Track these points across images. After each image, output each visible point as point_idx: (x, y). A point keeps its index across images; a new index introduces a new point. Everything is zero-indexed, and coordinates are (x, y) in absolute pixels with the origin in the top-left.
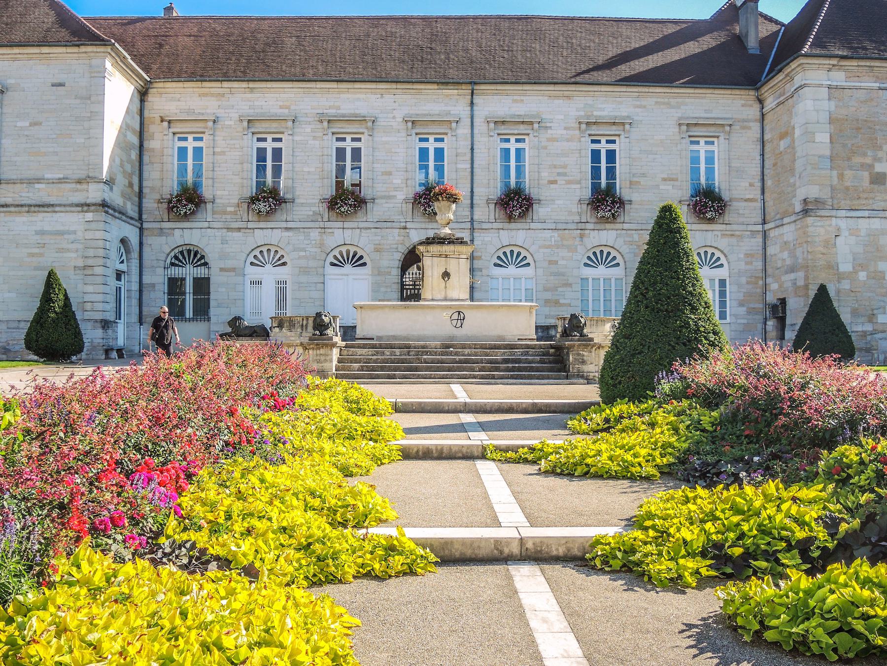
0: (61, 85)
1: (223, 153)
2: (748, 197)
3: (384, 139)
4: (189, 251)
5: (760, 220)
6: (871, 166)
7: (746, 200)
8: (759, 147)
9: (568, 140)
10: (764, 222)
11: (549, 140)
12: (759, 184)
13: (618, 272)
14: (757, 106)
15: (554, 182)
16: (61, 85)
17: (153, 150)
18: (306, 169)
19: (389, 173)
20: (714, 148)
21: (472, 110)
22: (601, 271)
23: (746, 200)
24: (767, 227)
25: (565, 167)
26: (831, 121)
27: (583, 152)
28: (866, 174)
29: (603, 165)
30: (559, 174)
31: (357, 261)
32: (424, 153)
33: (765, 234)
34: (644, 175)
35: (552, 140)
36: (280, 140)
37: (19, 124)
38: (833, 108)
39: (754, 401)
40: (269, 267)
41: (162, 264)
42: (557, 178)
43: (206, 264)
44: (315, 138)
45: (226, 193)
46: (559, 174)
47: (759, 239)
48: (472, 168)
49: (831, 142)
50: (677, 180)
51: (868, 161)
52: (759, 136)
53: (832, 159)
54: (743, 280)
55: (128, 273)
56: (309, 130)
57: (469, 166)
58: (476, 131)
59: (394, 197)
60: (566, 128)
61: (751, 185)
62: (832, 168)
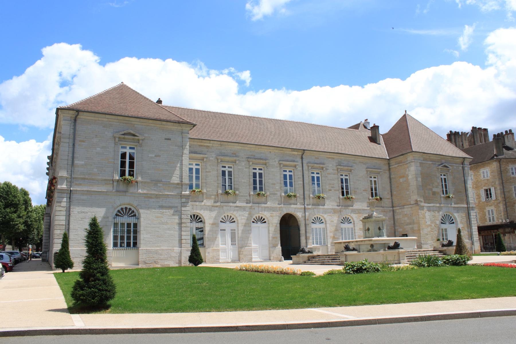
5: (391, 206)
6: (431, 189)
15: (330, 190)
18: (243, 181)
19: (274, 184)
21: (302, 160)
25: (333, 184)
28: (431, 192)
29: (258, 179)
30: (332, 187)
31: (262, 220)
32: (224, 173)
33: (393, 211)
37: (150, 155)
39: (112, 283)
42: (332, 189)
44: (246, 168)
45: (211, 189)
46: (332, 187)
47: (392, 213)
51: (431, 187)
56: (243, 164)
57: (302, 183)
59: (276, 194)
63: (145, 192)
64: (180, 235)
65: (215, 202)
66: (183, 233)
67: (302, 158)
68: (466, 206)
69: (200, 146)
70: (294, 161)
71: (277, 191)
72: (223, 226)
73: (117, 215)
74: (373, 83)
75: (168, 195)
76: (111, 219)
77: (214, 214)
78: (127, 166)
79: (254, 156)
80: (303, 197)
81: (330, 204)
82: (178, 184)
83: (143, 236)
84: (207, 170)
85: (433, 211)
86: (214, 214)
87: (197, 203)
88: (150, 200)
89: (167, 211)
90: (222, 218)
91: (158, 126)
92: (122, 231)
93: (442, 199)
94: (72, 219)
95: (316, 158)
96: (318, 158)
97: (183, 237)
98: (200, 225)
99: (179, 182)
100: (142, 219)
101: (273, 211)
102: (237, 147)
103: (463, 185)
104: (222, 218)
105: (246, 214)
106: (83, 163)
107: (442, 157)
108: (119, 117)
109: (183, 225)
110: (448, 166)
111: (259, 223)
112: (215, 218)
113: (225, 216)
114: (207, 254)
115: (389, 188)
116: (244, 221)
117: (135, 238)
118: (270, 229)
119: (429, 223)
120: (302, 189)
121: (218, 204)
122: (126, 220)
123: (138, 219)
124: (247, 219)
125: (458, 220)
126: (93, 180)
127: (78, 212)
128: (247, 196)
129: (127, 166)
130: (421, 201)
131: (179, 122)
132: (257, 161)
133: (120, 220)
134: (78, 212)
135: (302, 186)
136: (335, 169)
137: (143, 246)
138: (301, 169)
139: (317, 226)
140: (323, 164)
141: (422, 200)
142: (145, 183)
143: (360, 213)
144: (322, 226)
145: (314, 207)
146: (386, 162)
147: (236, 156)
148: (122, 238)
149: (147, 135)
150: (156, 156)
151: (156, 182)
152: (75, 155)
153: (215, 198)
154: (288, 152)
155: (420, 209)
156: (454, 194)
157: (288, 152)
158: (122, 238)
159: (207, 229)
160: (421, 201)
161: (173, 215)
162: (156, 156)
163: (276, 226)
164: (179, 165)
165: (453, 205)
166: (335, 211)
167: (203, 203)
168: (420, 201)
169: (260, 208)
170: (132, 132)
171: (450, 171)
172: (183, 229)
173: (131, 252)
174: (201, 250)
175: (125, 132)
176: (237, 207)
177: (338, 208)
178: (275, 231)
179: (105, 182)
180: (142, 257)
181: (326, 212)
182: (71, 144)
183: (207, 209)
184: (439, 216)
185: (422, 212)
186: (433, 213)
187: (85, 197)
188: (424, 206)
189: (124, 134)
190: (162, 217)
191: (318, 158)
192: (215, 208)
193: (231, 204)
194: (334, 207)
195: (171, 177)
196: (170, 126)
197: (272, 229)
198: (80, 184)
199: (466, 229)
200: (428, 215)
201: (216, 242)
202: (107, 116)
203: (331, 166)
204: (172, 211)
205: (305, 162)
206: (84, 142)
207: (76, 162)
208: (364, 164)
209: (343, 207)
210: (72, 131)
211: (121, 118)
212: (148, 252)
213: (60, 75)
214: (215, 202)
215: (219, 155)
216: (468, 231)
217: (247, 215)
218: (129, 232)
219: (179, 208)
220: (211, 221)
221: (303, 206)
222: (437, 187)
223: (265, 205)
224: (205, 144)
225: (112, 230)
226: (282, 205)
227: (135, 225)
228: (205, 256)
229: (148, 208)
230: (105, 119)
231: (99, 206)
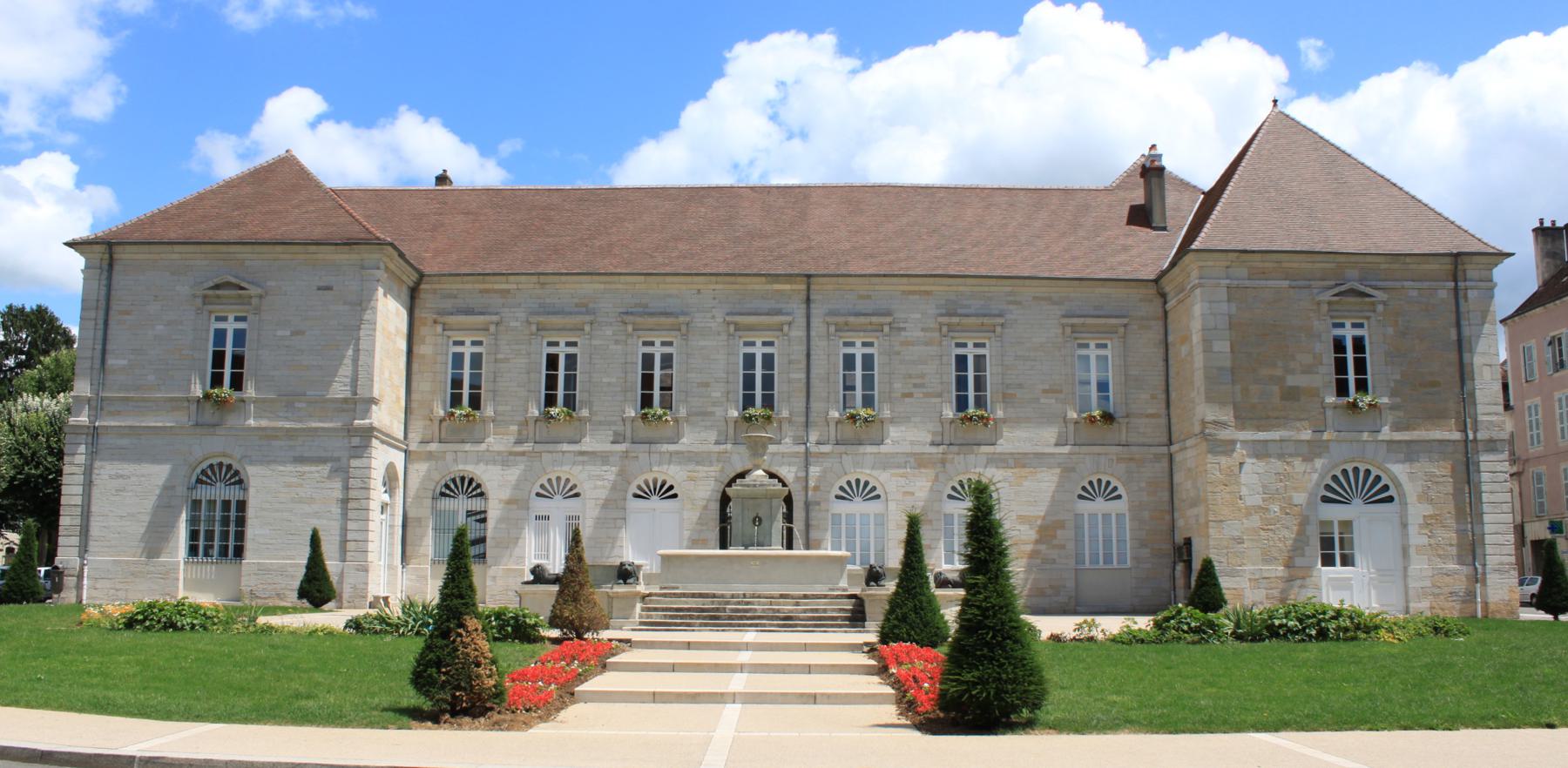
0: (329, 288)
1: (506, 360)
2: (1150, 411)
3: (702, 343)
4: (463, 479)
5: (1165, 440)
6: (1281, 380)
7: (1148, 416)
8: (1162, 350)
9: (926, 344)
10: (1170, 443)
11: (903, 344)
12: (1164, 396)
13: (1120, 506)
14: (1159, 301)
15: (910, 395)
16: (329, 288)
17: (423, 356)
19: (707, 385)
20: (1107, 352)
21: (808, 308)
22: (1100, 506)
23: (1148, 416)
24: (1174, 448)
25: (922, 376)
26: (1231, 326)
27: (945, 359)
28: (1276, 389)
30: (915, 386)
31: (667, 492)
34: (1020, 386)
35: (906, 343)
36: (574, 344)
37: (280, 333)
38: (1234, 310)
40: (1357, 501)
41: (430, 494)
43: (482, 494)
44: (617, 342)
46: (915, 386)
47: (1165, 464)
48: (808, 378)
49: (1232, 351)
50: (1061, 392)
51: (1279, 372)
52: (1162, 337)
53: (1233, 370)
54: (1146, 515)
55: (393, 506)
56: (609, 333)
57: (803, 376)
58: (813, 333)
59: (712, 414)
60: (923, 330)
61: (1153, 397)
62: (1233, 382)
63: (264, 423)
64: (344, 530)
65: (519, 442)
66: (351, 525)
67: (808, 301)
68: (1457, 436)
69: (481, 291)
70: (779, 312)
71: (714, 404)
72: (541, 506)
73: (199, 481)
74: (926, 44)
75: (316, 429)
76: (181, 490)
77: (514, 474)
78: (228, 368)
79: (646, 306)
80: (803, 419)
81: (906, 436)
82: (345, 400)
83: (254, 530)
84: (500, 356)
85: (1281, 456)
86: (514, 474)
87: (468, 447)
88: (274, 443)
89: (313, 468)
90: (542, 486)
91: (302, 256)
92: (211, 520)
93: (1329, 413)
94: (96, 492)
95: (861, 297)
96: (869, 297)
97: (350, 536)
98: (476, 505)
99: (348, 394)
100: (252, 491)
101: (698, 463)
102: (588, 287)
103: (1453, 356)
104: (542, 486)
105: (610, 473)
106: (125, 362)
107: (1342, 259)
108: (204, 248)
109: (351, 505)
110: (1368, 290)
111: (655, 498)
112: (517, 487)
113: (549, 480)
114: (489, 583)
115: (1158, 380)
116: (603, 494)
117: (240, 536)
118: (686, 515)
119: (1257, 500)
120: (804, 394)
121: (527, 447)
122: (220, 492)
123: (245, 490)
124: (614, 488)
125: (1411, 490)
126: (144, 400)
127: (111, 477)
128: (614, 423)
129: (228, 368)
130: (1223, 425)
131: (349, 243)
132: (651, 321)
133: (204, 493)
134: (111, 477)
135: (802, 385)
136: (932, 324)
137: (250, 558)
138: (802, 333)
139: (857, 507)
140: (888, 313)
141: (1227, 415)
142: (264, 401)
143: (1024, 466)
144: (873, 507)
145: (842, 448)
146: (1152, 291)
147: (588, 313)
148: (210, 535)
149: (273, 283)
150: (294, 333)
151: (289, 400)
152: (109, 347)
153: (520, 433)
154: (757, 287)
155: (1211, 451)
156: (1393, 394)
157: (757, 287)
158: (210, 535)
159: (492, 516)
160: (1223, 425)
161: (329, 478)
162: (293, 334)
163: (705, 508)
164: (350, 352)
165: (1386, 433)
166: (920, 461)
167: (483, 447)
168: (1215, 423)
169: (655, 457)
170: (233, 280)
171: (1380, 308)
172: (351, 514)
173: (228, 567)
174: (476, 569)
175: (217, 281)
176: (582, 453)
177: (934, 450)
178: (701, 521)
179: (174, 404)
180: (248, 582)
181: (885, 463)
182: (101, 322)
183: (495, 462)
184: (1310, 475)
185: (1224, 460)
186: (1278, 465)
187: (124, 442)
188: (1233, 442)
189: (217, 287)
190: (301, 485)
191: (869, 297)
192: (519, 458)
193: (565, 447)
194: (917, 449)
195: (330, 384)
196: (327, 254)
197: (692, 516)
198: (119, 413)
199: (1451, 522)
200: (1253, 473)
201: (517, 551)
202: (177, 248)
203: (917, 318)
204: (325, 469)
205: (817, 310)
206: (127, 313)
207: (110, 362)
208: (1055, 303)
209: (955, 449)
210: (103, 292)
211: (209, 248)
212: (263, 570)
213: (314, 124)
214: (519, 442)
215: (538, 314)
216: (1461, 533)
217: (612, 477)
218: (225, 521)
219: (344, 460)
220: (506, 494)
221: (802, 448)
222: (1308, 370)
223: (672, 448)
224: (496, 287)
225: (184, 516)
226: (729, 446)
227: (242, 506)
228: (485, 587)
229: (267, 460)
230: (175, 256)
231: (155, 460)
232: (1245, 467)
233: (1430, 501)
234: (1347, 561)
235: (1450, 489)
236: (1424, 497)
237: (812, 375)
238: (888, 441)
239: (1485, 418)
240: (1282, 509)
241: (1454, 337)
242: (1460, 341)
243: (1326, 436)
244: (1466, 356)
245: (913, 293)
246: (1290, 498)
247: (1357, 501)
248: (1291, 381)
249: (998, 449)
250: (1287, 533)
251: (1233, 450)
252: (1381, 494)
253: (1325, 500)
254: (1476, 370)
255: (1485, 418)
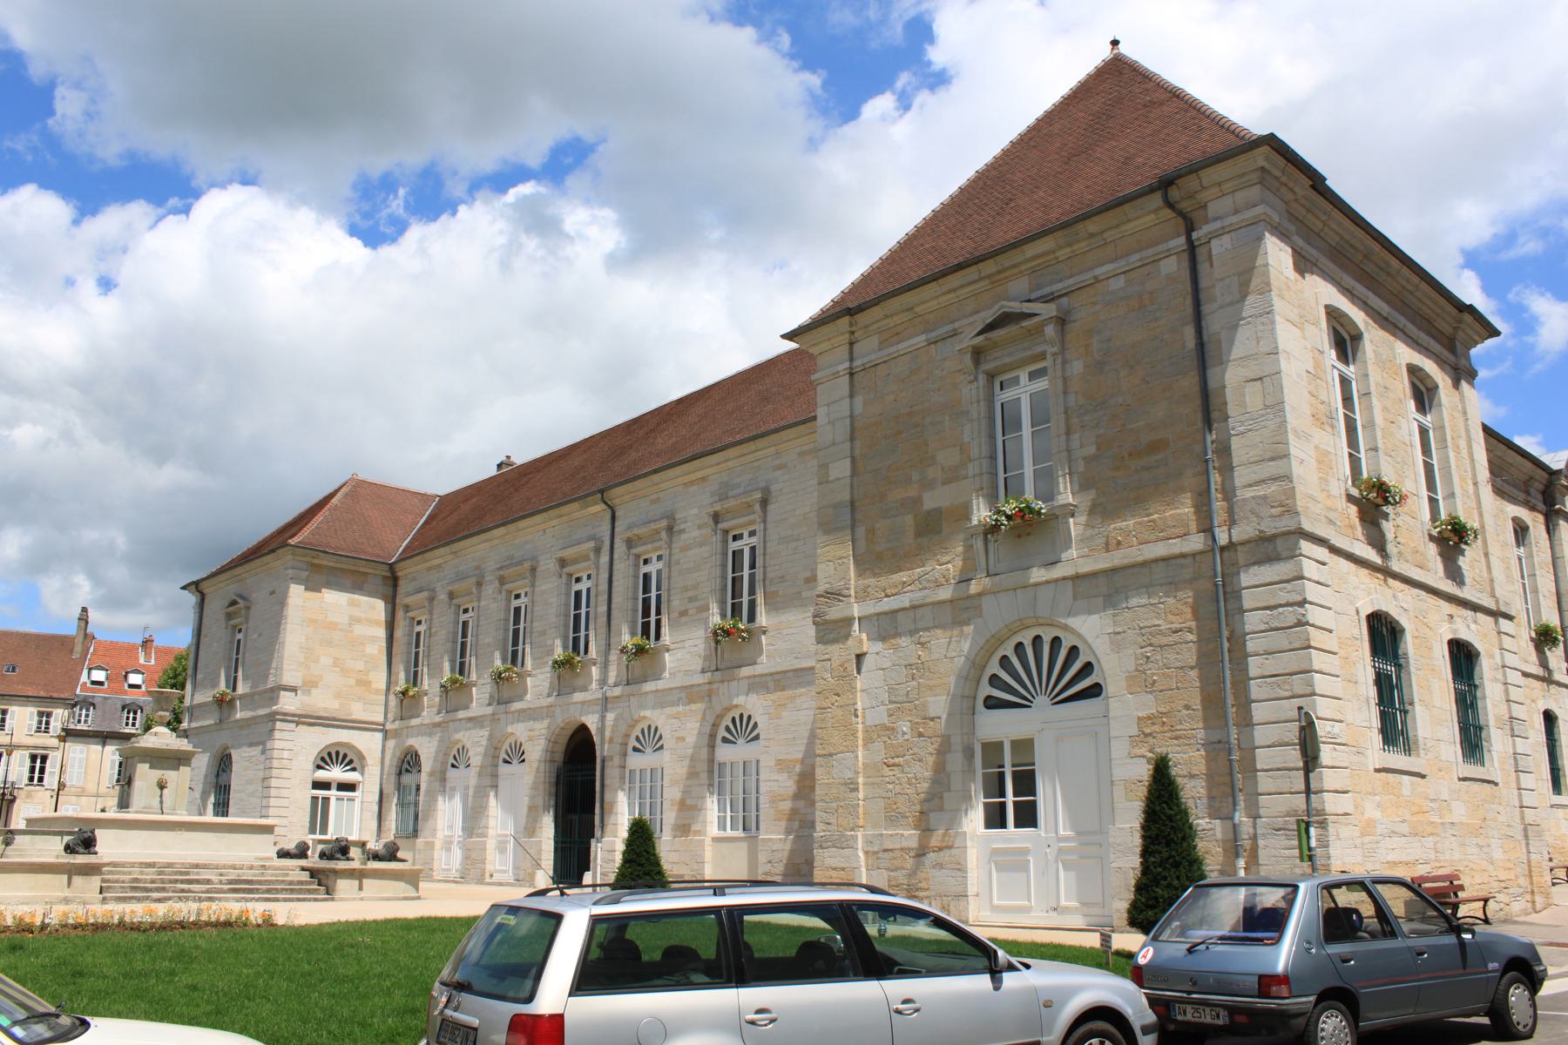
6: (918, 500)
28: (909, 520)
40: (1042, 701)
51: (912, 492)
79: (512, 557)
119: (880, 716)
125: (1113, 668)
194: (688, 681)
232: (868, 663)
233: (1150, 686)
234: (1027, 817)
235: (1190, 656)
236: (1141, 681)
237: (614, 606)
238: (666, 674)
239: (1249, 493)
240: (914, 726)
241: (1191, 343)
242: (1201, 345)
243: (974, 588)
244: (1212, 374)
245: (692, 483)
246: (924, 705)
247: (1042, 701)
248: (930, 501)
249: (758, 669)
250: (917, 768)
251: (847, 636)
252: (1080, 684)
253: (992, 704)
254: (1229, 393)
255: (1249, 493)
